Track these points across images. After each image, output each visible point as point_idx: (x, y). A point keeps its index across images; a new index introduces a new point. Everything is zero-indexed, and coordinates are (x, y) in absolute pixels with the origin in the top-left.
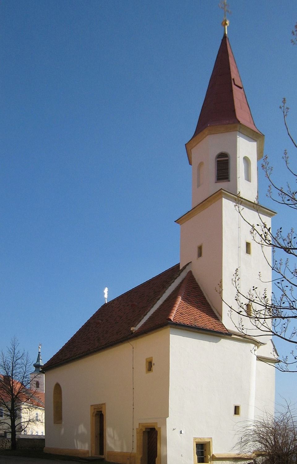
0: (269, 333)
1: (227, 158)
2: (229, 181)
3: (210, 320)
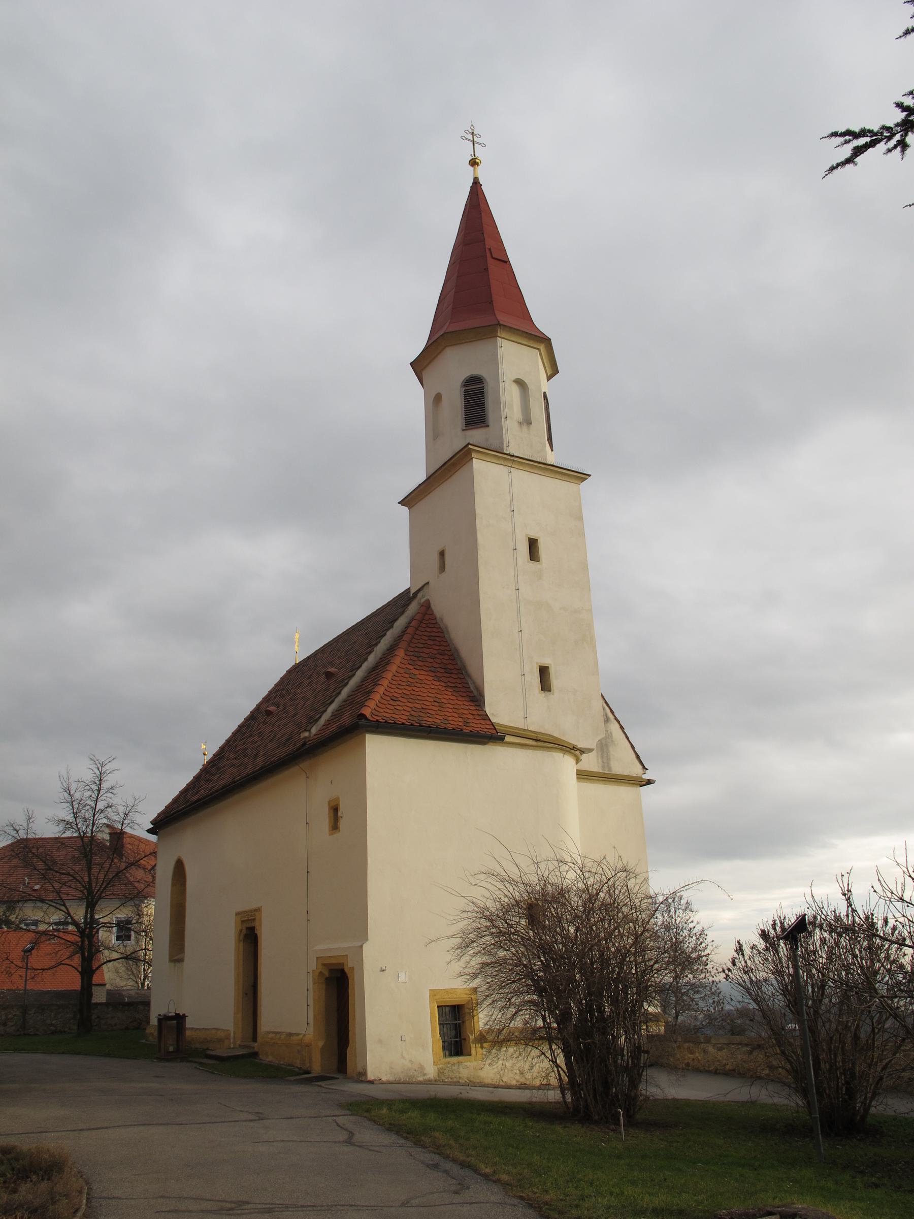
0: (530, 743)
1: (482, 386)
2: (488, 426)
3: (457, 707)
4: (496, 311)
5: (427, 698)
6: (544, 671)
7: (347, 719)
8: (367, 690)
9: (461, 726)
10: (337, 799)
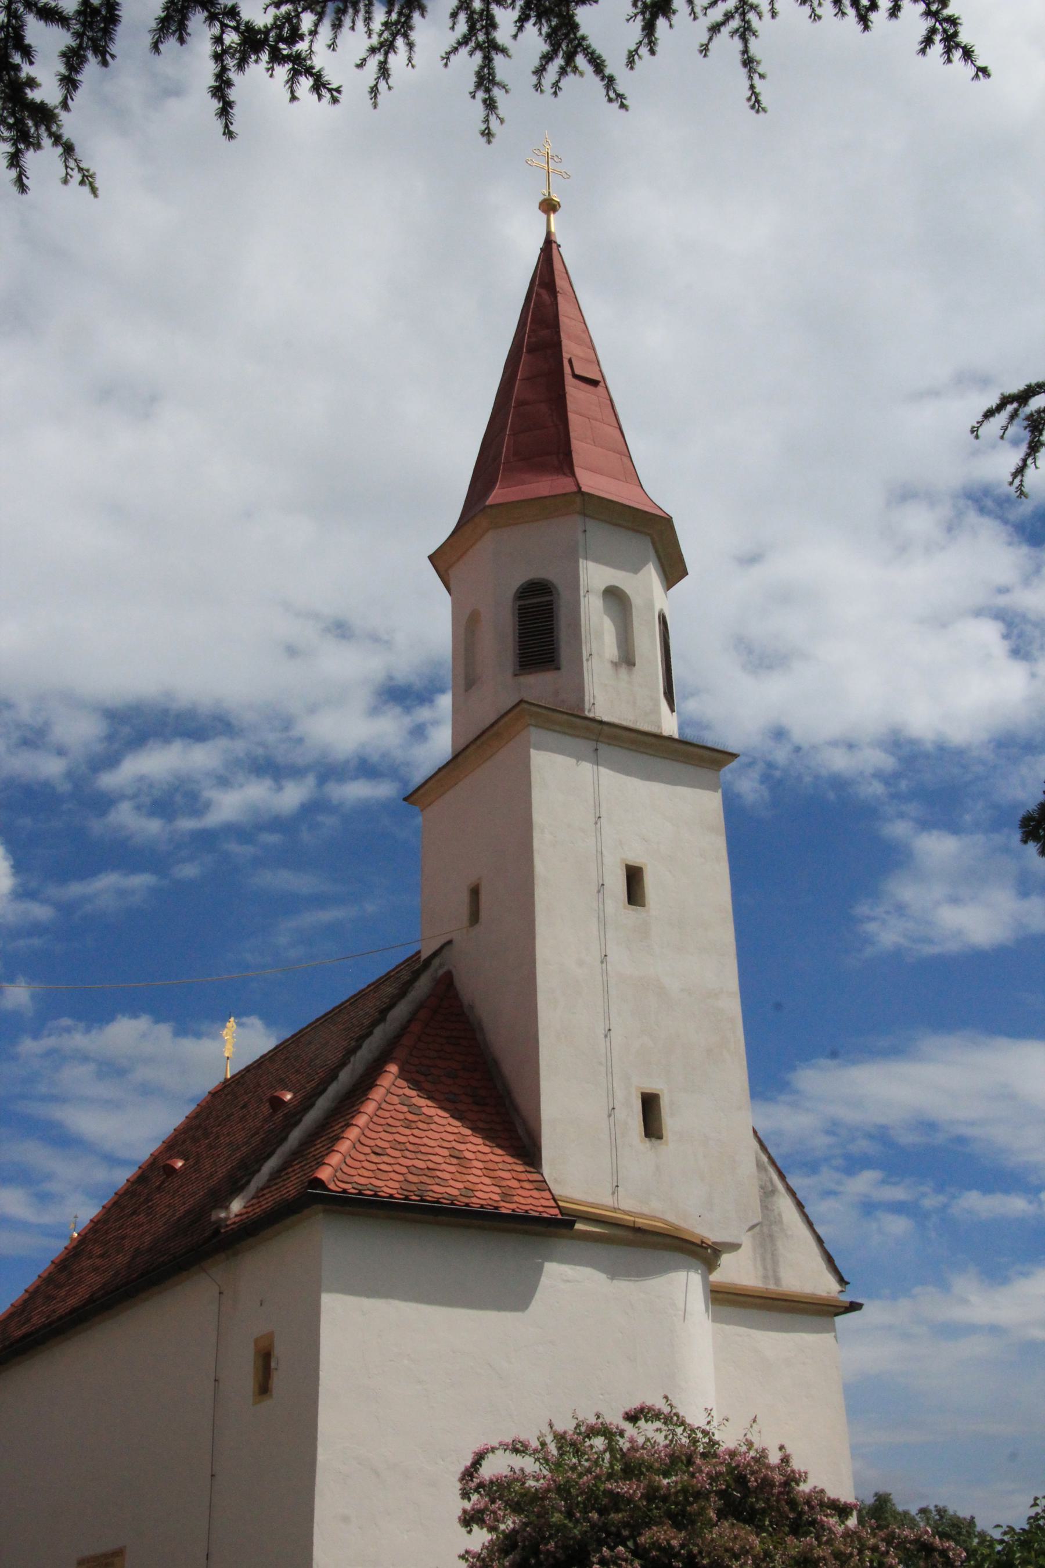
2: (558, 669)
3: (491, 1166)
4: (578, 471)
5: (438, 1150)
6: (650, 1104)
7: (291, 1187)
8: (332, 1135)
9: (495, 1201)
10: (270, 1336)
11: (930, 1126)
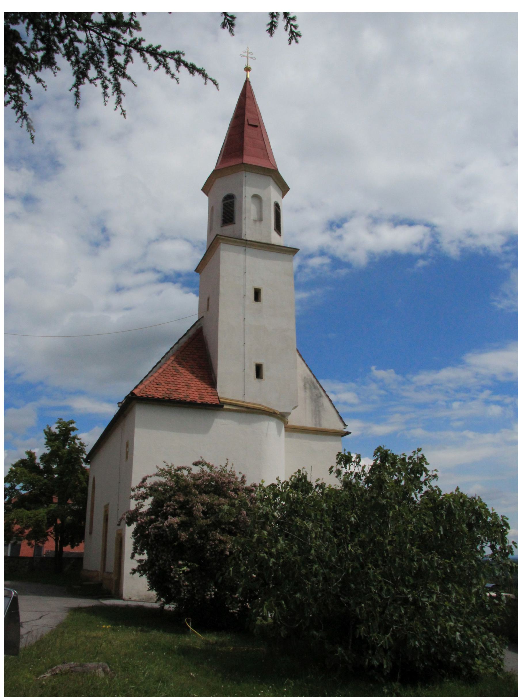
1: (232, 200)
2: (235, 223)
3: (199, 388)
11: (509, 374)
